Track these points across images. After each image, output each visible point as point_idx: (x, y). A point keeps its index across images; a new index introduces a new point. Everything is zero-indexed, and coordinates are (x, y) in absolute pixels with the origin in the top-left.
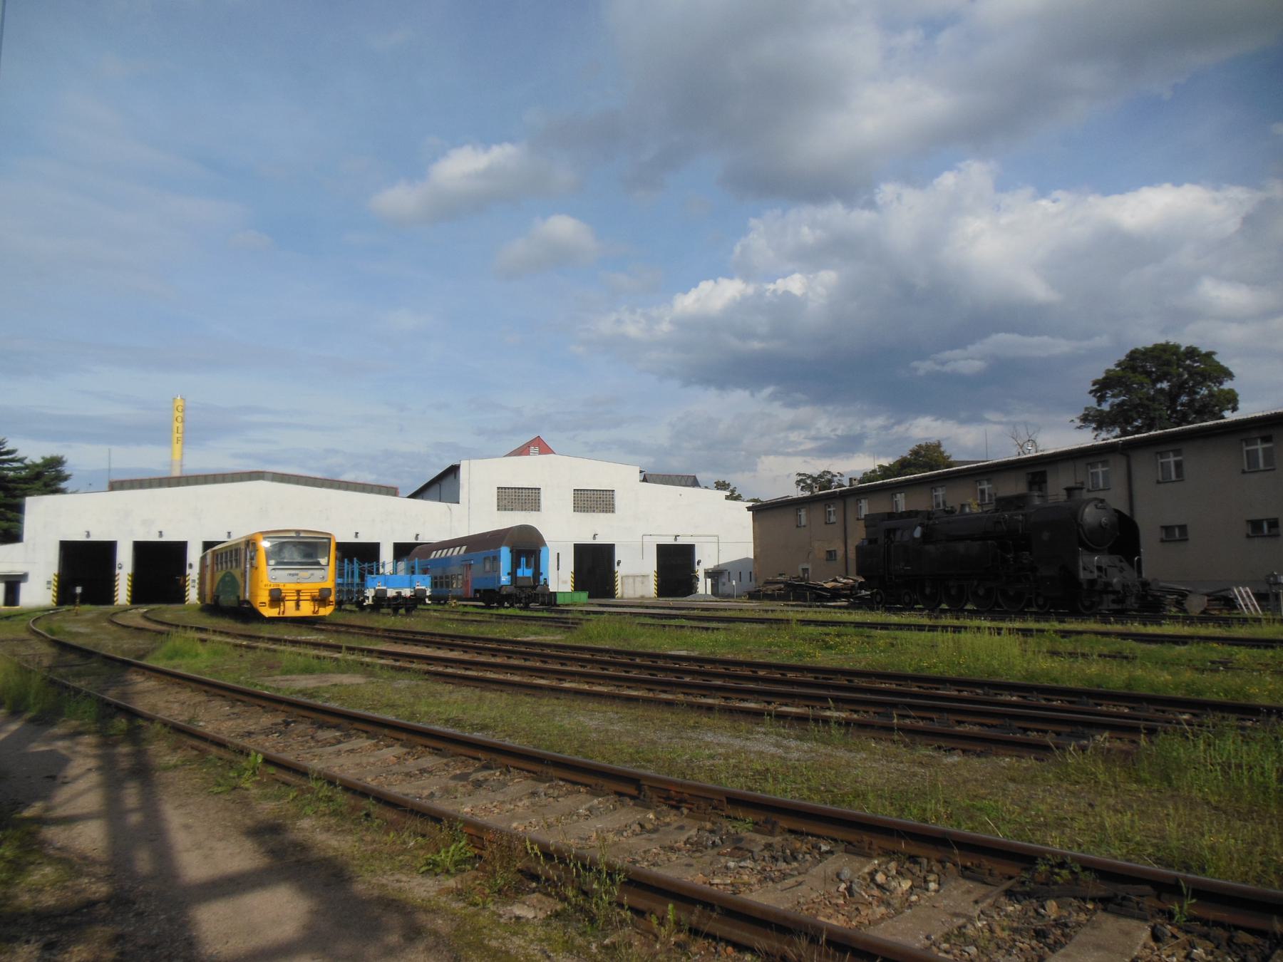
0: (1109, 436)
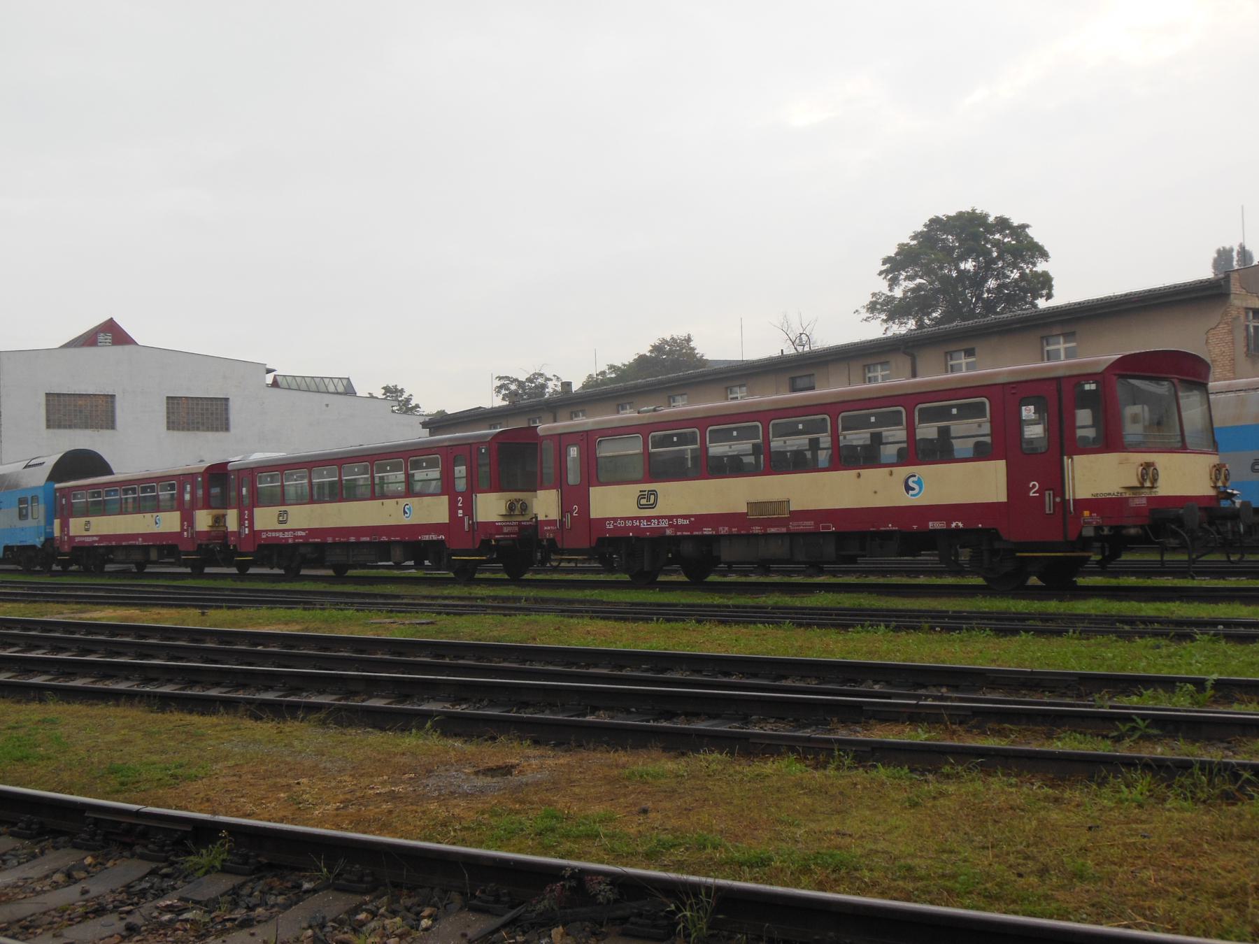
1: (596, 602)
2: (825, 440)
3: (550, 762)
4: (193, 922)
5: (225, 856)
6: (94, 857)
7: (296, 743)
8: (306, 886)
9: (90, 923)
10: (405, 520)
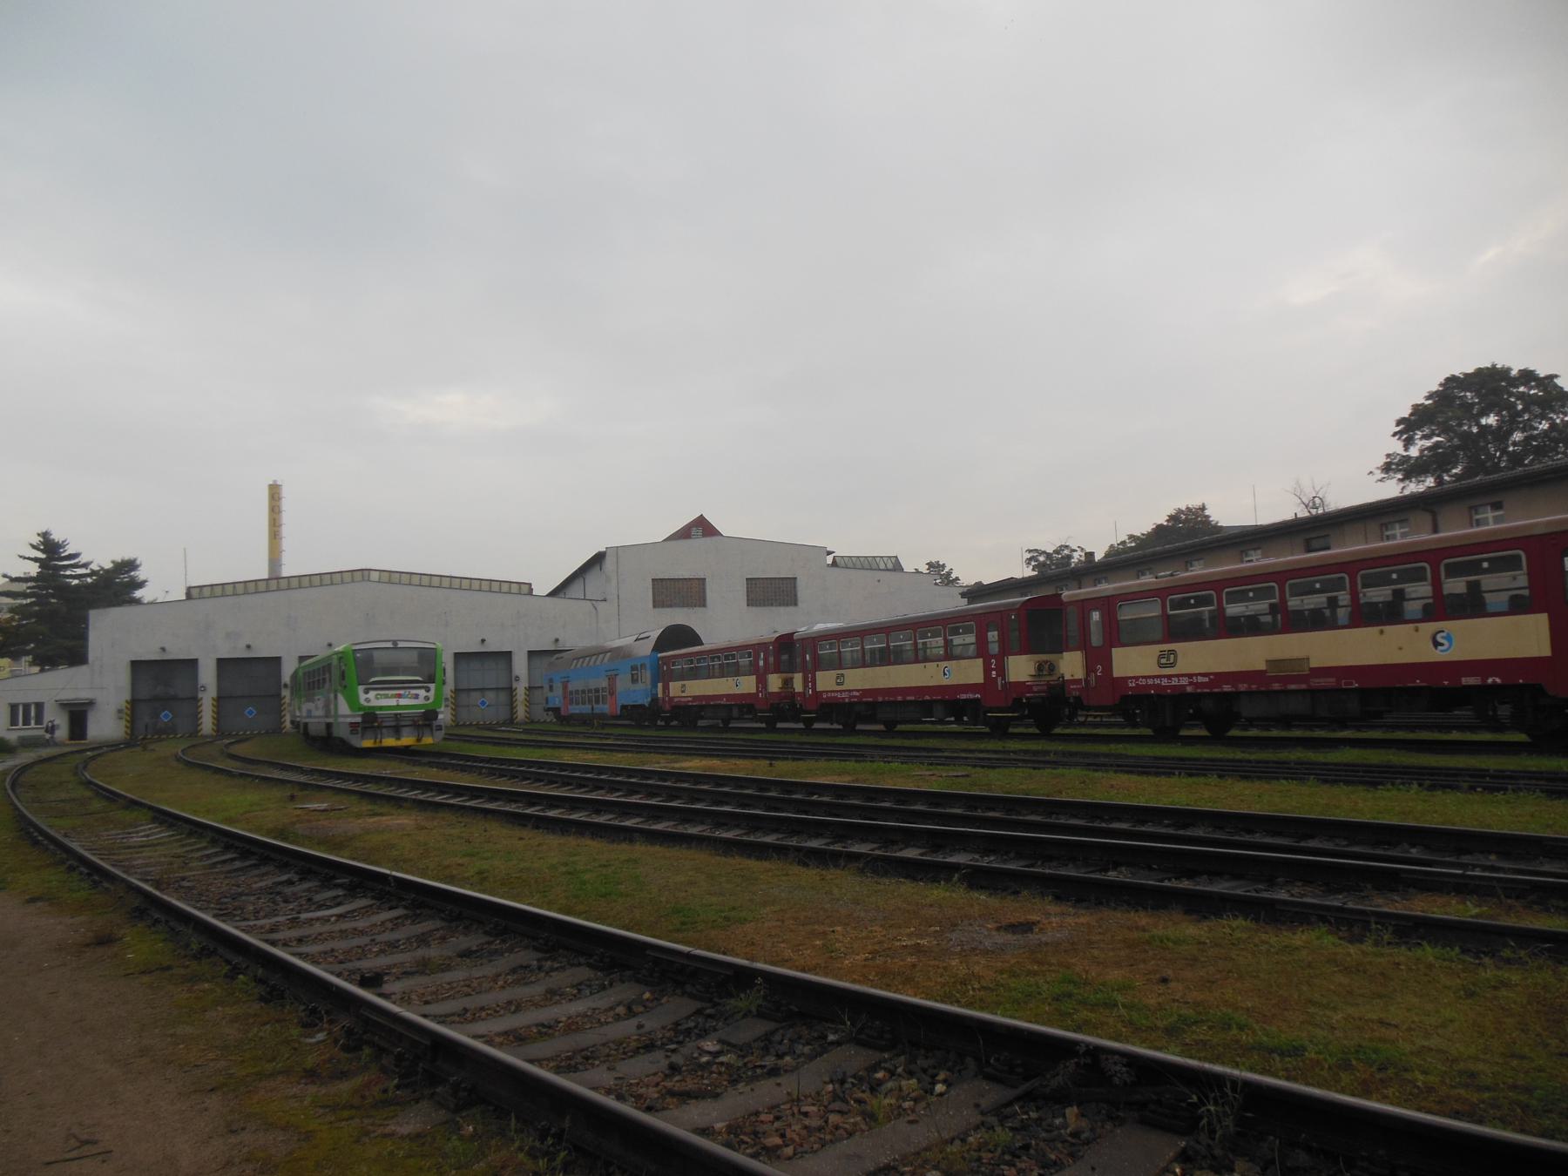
0: (1413, 487)
1: (1120, 756)
2: (1344, 597)
3: (1069, 920)
4: (728, 1066)
5: (760, 1002)
6: (652, 993)
7: (836, 891)
8: (831, 1037)
9: (640, 1057)
10: (945, 681)
